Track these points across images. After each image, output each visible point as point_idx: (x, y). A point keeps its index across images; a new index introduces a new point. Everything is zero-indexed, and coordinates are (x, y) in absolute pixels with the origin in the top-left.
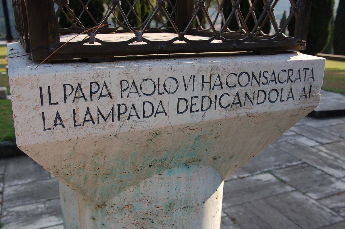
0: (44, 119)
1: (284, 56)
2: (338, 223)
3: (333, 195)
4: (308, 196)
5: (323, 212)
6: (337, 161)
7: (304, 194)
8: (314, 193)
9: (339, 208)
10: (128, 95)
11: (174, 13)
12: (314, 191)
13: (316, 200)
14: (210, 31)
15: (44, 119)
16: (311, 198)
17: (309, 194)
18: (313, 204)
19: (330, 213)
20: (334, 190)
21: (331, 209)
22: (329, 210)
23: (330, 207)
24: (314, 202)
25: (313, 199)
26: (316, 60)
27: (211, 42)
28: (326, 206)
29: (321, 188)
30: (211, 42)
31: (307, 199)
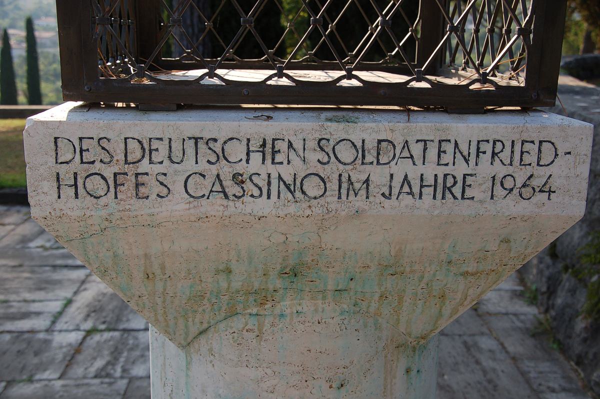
0: (470, 145)
1: (108, 113)
2: (127, 388)
3: (73, 357)
4: (41, 380)
5: (93, 388)
6: (11, 307)
7: (30, 380)
8: (45, 370)
9: (104, 368)
10: (104, 195)
11: (467, 58)
12: (42, 367)
13: (59, 378)
14: (202, 82)
15: (470, 145)
16: (50, 380)
17: (37, 377)
18: (63, 386)
19: (102, 383)
20: (64, 350)
21: (96, 377)
22: (97, 381)
23: (92, 375)
24: (60, 383)
25: (55, 380)
26: (60, 121)
27: (338, 85)
28: (85, 377)
29: (45, 357)
30: (338, 85)
31: (46, 386)
